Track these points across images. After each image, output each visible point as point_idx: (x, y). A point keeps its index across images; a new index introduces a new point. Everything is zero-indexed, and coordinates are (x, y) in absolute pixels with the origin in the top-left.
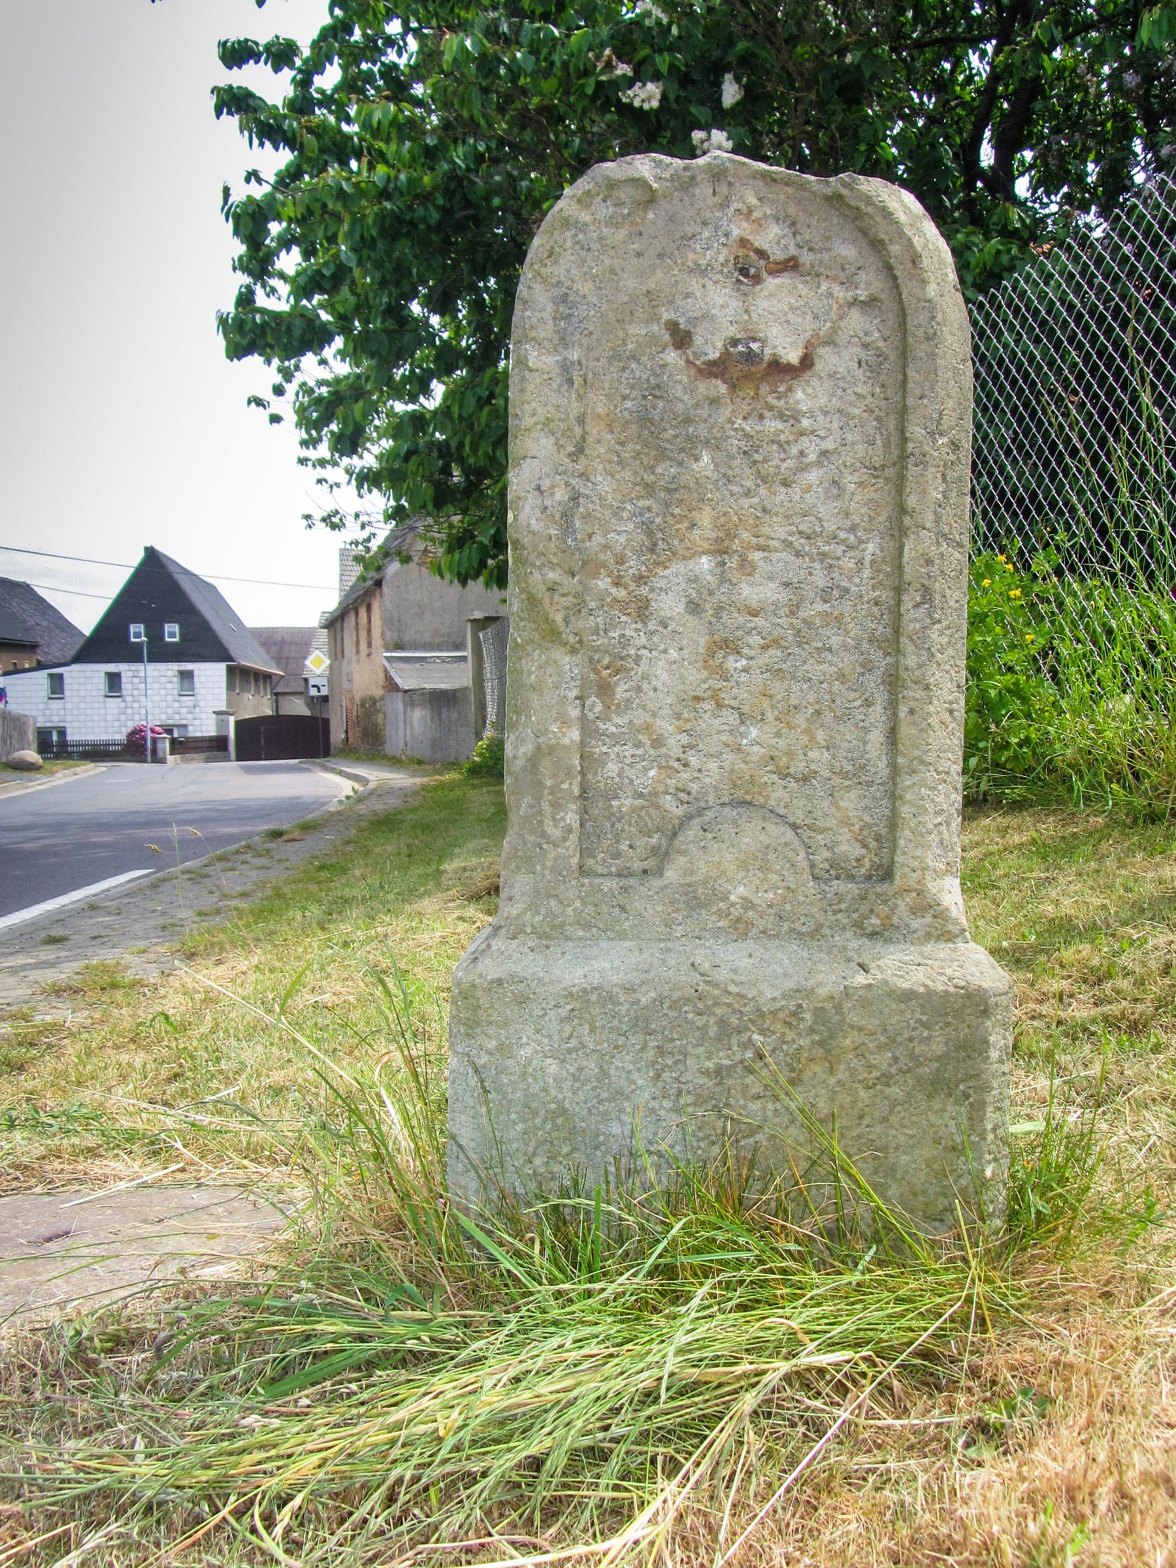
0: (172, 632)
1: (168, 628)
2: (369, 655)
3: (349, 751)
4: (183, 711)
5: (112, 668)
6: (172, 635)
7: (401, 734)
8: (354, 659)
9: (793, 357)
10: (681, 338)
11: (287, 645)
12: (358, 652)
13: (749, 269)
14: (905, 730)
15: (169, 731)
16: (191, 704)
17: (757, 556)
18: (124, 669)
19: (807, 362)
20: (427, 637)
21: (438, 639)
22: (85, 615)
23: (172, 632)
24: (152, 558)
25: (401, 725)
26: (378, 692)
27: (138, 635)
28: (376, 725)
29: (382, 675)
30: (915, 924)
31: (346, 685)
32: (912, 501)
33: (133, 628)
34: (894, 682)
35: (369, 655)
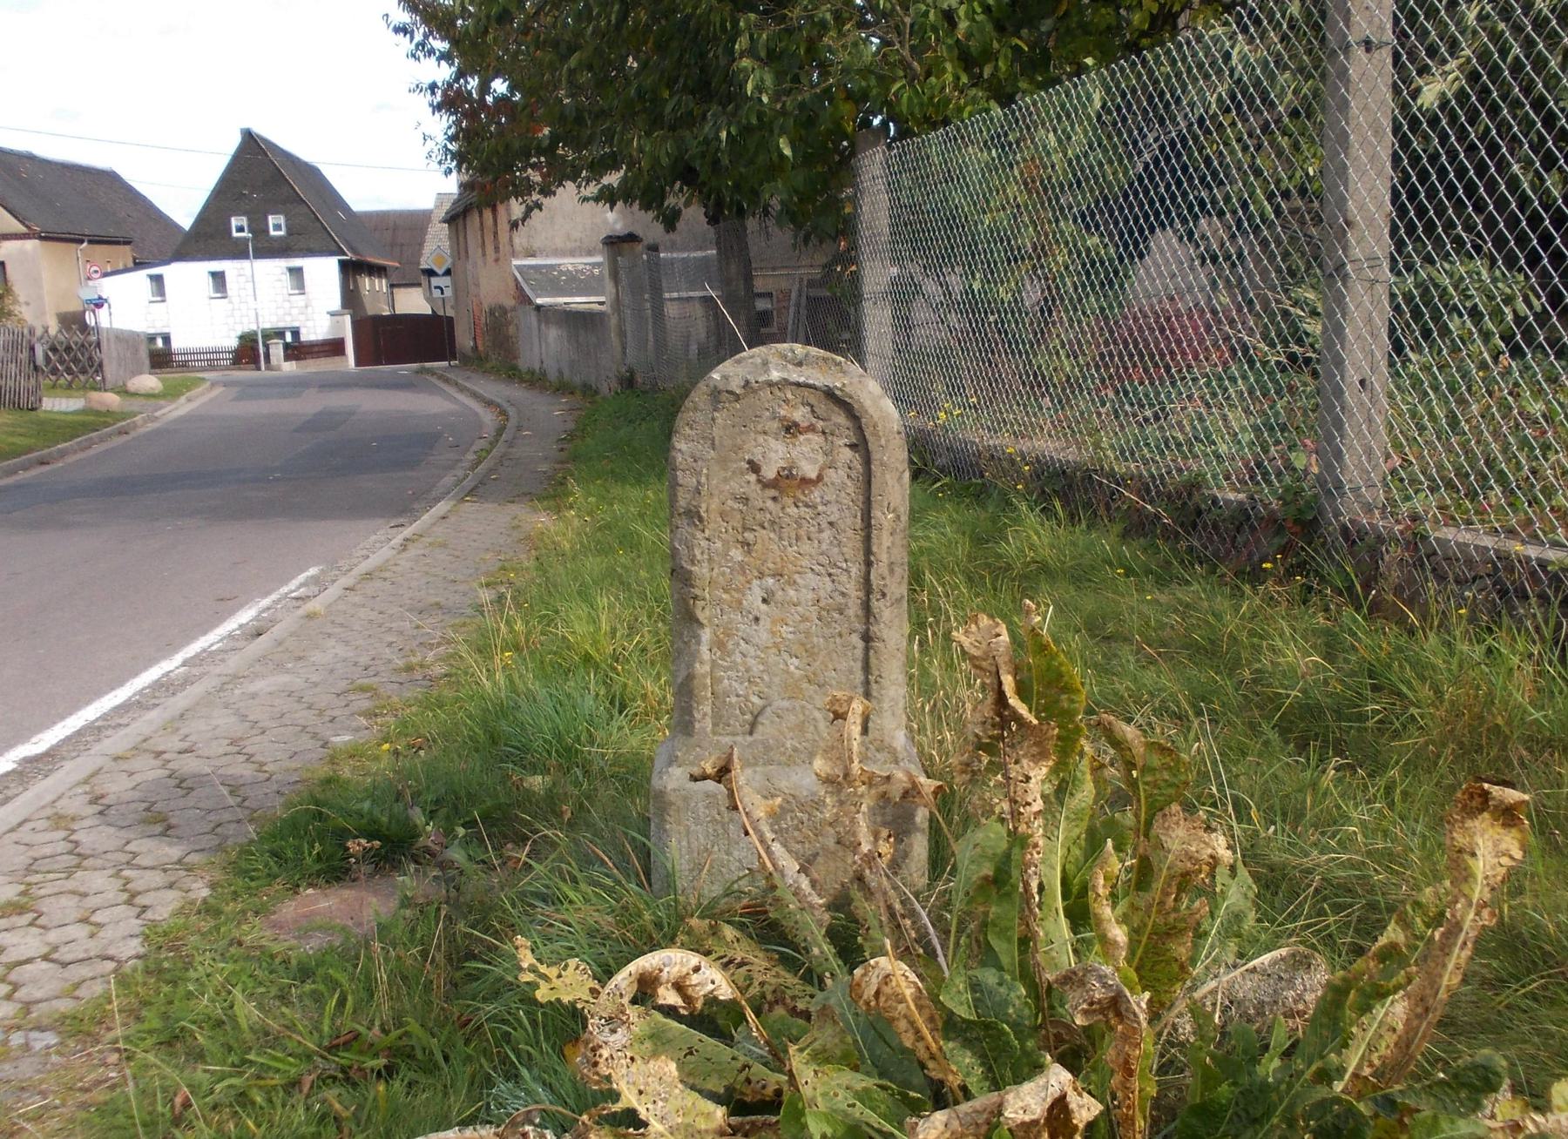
0: (276, 225)
1: (272, 220)
2: (497, 260)
3: (475, 361)
4: (294, 311)
5: (216, 266)
6: (278, 227)
7: (536, 349)
8: (480, 262)
9: (813, 476)
10: (754, 467)
11: (402, 229)
12: (484, 255)
13: (791, 429)
14: (873, 661)
15: (280, 334)
16: (302, 304)
17: (796, 576)
18: (228, 266)
19: (820, 478)
20: (559, 242)
21: (569, 245)
22: (184, 213)
23: (276, 225)
24: (252, 145)
25: (536, 340)
26: (509, 302)
27: (240, 229)
28: (507, 338)
29: (512, 285)
30: (878, 756)
31: (472, 288)
32: (874, 549)
33: (234, 222)
34: (867, 638)
35: (497, 260)
